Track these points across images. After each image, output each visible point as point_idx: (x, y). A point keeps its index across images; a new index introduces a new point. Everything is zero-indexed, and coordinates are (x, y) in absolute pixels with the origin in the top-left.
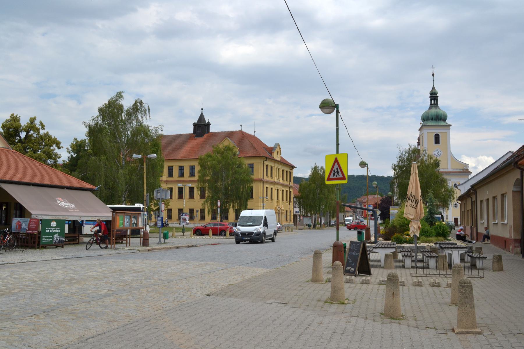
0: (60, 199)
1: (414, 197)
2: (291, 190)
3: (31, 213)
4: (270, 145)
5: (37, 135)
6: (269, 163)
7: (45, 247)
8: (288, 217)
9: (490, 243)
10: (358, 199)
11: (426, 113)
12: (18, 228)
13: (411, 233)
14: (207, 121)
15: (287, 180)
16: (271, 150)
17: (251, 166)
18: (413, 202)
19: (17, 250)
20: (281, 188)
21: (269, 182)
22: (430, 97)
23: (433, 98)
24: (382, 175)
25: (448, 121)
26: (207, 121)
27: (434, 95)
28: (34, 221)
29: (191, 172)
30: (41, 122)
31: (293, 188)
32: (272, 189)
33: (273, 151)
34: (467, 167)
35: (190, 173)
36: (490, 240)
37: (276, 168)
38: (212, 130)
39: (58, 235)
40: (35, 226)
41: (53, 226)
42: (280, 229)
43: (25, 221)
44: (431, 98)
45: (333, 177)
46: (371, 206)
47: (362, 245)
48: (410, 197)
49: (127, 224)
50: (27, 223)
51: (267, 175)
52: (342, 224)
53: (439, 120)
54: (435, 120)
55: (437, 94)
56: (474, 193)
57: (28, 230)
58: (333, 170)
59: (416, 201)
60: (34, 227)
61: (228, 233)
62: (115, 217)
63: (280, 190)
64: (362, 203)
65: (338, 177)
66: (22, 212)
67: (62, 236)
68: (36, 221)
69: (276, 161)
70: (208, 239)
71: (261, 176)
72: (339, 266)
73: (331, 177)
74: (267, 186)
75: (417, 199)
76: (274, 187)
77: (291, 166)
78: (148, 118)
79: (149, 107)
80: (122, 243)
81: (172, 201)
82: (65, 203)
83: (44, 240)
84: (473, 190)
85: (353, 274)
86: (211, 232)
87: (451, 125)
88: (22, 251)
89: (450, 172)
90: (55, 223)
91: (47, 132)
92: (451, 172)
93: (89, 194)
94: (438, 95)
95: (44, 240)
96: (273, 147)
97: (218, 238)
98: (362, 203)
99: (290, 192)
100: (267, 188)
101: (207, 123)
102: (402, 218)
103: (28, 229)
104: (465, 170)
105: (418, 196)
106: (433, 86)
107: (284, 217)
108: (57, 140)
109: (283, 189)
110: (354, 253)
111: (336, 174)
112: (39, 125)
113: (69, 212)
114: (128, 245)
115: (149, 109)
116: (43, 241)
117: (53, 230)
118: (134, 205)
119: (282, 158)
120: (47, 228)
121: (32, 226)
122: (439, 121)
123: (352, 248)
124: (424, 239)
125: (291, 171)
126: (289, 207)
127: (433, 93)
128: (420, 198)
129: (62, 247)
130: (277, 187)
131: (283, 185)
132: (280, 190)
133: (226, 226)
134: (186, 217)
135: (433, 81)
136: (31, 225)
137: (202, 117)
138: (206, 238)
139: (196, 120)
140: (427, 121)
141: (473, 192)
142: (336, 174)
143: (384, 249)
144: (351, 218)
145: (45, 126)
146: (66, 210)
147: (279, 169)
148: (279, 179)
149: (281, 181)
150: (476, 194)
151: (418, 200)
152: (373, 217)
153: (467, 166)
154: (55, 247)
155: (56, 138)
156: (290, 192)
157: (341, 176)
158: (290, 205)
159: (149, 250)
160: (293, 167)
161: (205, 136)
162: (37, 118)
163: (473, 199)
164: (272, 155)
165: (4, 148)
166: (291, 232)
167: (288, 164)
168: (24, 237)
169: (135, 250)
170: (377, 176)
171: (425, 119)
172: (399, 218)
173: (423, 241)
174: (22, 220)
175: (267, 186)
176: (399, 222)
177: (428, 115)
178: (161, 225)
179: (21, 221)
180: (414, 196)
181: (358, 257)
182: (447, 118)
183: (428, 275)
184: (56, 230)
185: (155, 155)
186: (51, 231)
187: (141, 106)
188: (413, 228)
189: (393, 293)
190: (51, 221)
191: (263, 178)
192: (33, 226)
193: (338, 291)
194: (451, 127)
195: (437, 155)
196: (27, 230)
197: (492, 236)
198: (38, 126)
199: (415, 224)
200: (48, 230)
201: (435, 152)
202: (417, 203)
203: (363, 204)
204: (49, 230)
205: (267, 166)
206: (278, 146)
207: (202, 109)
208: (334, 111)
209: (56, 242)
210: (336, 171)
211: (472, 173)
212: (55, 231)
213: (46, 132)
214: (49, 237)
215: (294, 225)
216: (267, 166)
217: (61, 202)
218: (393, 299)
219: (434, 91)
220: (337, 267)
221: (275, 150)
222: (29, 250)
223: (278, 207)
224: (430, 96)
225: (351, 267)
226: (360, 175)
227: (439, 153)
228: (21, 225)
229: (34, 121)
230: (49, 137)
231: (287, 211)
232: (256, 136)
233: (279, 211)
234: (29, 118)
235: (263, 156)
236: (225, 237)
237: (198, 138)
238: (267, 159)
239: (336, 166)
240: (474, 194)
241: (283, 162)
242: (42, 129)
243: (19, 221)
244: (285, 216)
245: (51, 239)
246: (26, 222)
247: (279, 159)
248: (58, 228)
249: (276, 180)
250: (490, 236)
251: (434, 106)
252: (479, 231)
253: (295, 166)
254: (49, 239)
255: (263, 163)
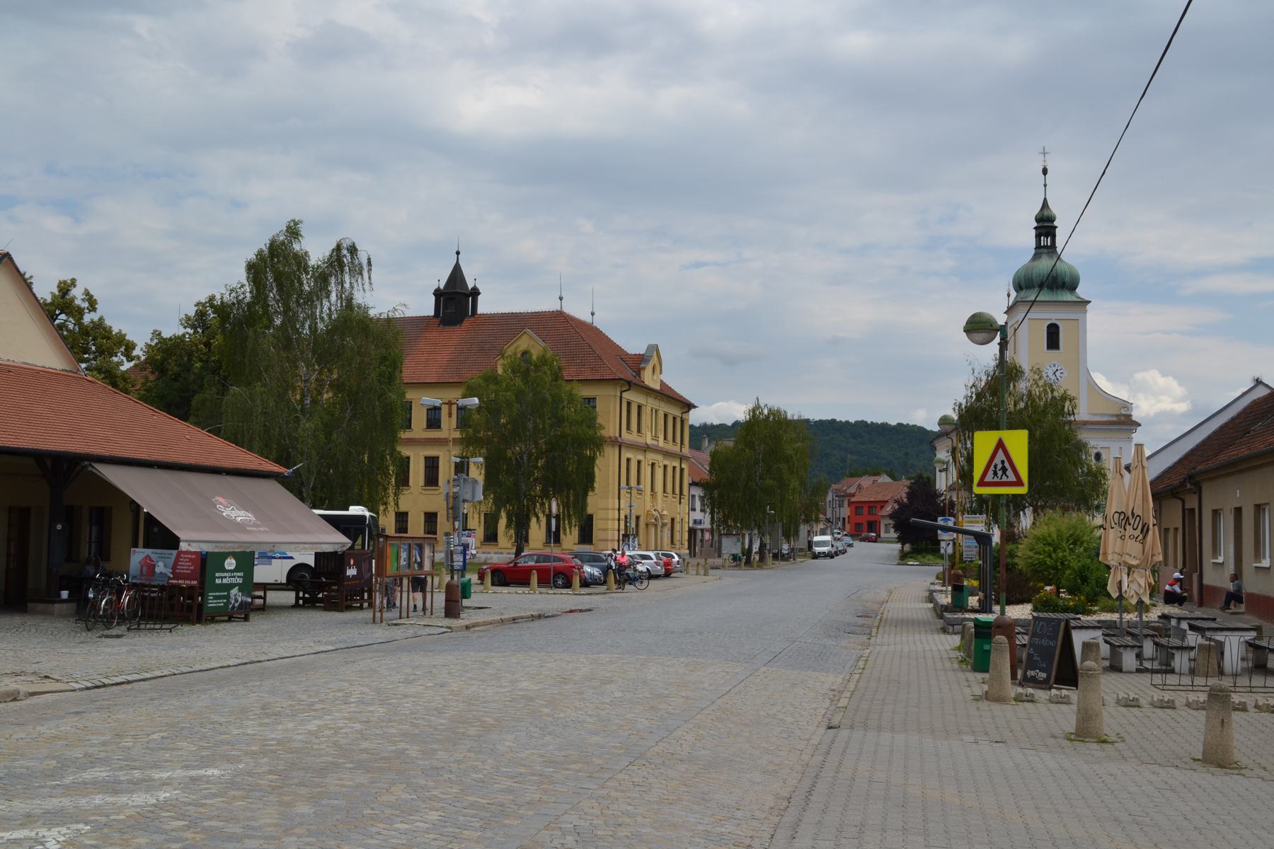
0: (221, 500)
1: (1138, 518)
2: (683, 466)
3: (179, 538)
4: (633, 345)
5: (75, 325)
6: (633, 396)
7: (212, 620)
8: (677, 536)
9: (1243, 613)
10: (833, 485)
11: (1026, 268)
12: (144, 573)
13: (1132, 596)
14: (470, 286)
15: (674, 440)
16: (638, 363)
17: (591, 401)
18: (1136, 529)
19: (158, 626)
20: (660, 460)
21: (634, 447)
22: (1035, 228)
23: (1044, 231)
24: (882, 422)
25: (1081, 291)
26: (470, 286)
27: (1046, 224)
28: (189, 556)
29: (429, 416)
30: (87, 293)
31: (687, 460)
32: (639, 462)
33: (641, 366)
34: (1128, 410)
35: (429, 421)
36: (1243, 606)
37: (650, 409)
38: (485, 306)
39: (240, 591)
40: (192, 568)
41: (230, 568)
42: (678, 569)
43: (162, 557)
44: (1039, 231)
45: (992, 480)
46: (949, 520)
47: (1063, 624)
48: (1131, 517)
49: (405, 563)
50: (171, 562)
51: (628, 428)
52: (804, 553)
53: (1057, 289)
54: (1048, 287)
55: (1054, 221)
56: (1195, 491)
57: (173, 579)
58: (993, 464)
59: (1143, 527)
60: (189, 572)
61: (576, 581)
62: (383, 547)
63: (659, 467)
64: (843, 496)
65: (1004, 479)
66: (164, 538)
67: (246, 592)
68: (194, 556)
69: (648, 391)
70: (524, 595)
71: (615, 429)
72: (1095, 670)
73: (989, 478)
74: (629, 455)
75: (1146, 524)
76: (645, 458)
77: (685, 403)
78: (367, 286)
79: (369, 259)
80: (361, 608)
81: (409, 492)
82: (233, 509)
83: (210, 601)
84: (1191, 484)
85: (1044, 686)
86: (534, 579)
87: (1090, 302)
88: (170, 629)
89: (1083, 421)
90: (234, 561)
91: (101, 319)
92: (1087, 422)
93: (273, 487)
94: (1055, 223)
95: (211, 603)
96: (643, 355)
97: (554, 594)
98: (843, 496)
99: (682, 470)
100: (628, 460)
101: (472, 289)
102: (1037, 550)
103: (171, 576)
104: (1123, 418)
105: (1149, 517)
106: (1045, 199)
107: (668, 534)
108: (127, 338)
109: (666, 462)
110: (1045, 642)
111: (1000, 473)
112: (83, 300)
113: (249, 532)
114: (428, 612)
115: (369, 263)
116: (210, 605)
117: (229, 577)
118: (348, 510)
119: (662, 383)
120: (217, 575)
121: (183, 569)
122: (1059, 292)
123: (1038, 630)
124: (1106, 603)
125: (684, 416)
126: (679, 508)
127: (1045, 218)
128: (1152, 521)
129: (246, 619)
130: (651, 457)
131: (667, 454)
132: (659, 467)
133: (567, 562)
134: (469, 538)
135: (1045, 186)
136: (181, 565)
137: (457, 275)
138: (524, 593)
139: (441, 278)
140: (1028, 291)
141: (1193, 487)
142: (1000, 473)
143: (1077, 630)
144: (828, 538)
145: (98, 302)
146: (241, 527)
147: (656, 411)
148: (655, 438)
149: (661, 443)
150: (1199, 492)
151: (1146, 526)
152: (873, 534)
153: (1128, 408)
154: (226, 618)
155: (123, 332)
156: (682, 470)
157: (1012, 478)
158: (680, 503)
159: (467, 627)
160: (688, 406)
161: (466, 323)
162: (77, 283)
163: (1186, 504)
164: (639, 375)
165: (66, 371)
166: (705, 575)
167: (671, 395)
168: (152, 595)
169: (442, 627)
170: (869, 422)
171: (1023, 285)
172: (1031, 551)
173: (1105, 608)
174: (156, 553)
175: (629, 455)
176: (1030, 561)
177: (1032, 275)
178: (461, 564)
179: (153, 557)
180: (1139, 516)
181: (1055, 649)
182: (1078, 284)
183: (1254, 690)
184: (234, 577)
185: (476, 400)
186: (225, 581)
187: (352, 258)
188: (1137, 585)
189: (1223, 720)
190: (225, 555)
191: (620, 436)
192: (187, 569)
193: (1094, 717)
194: (1089, 307)
195: (1053, 377)
196: (170, 578)
197: (1251, 596)
198: (78, 302)
199: (1142, 577)
200: (219, 578)
201: (1047, 371)
202: (1145, 530)
203: (847, 499)
204: (222, 578)
205: (629, 404)
206: (655, 353)
207: (458, 253)
208: (995, 337)
209: (234, 606)
210: (1000, 466)
211: (1140, 425)
212: (234, 581)
213: (96, 319)
214: (221, 594)
215: (691, 557)
216: (629, 404)
217: (226, 507)
218: (1223, 732)
219: (1046, 213)
220: (1090, 672)
221: (648, 364)
222: (183, 627)
223: (655, 510)
224: (1035, 224)
225: (1038, 671)
226: (824, 418)
227: (1058, 374)
228: (154, 566)
229: (68, 290)
230: (104, 329)
231: (673, 520)
232: (595, 325)
233: (655, 519)
234: (56, 283)
235: (621, 379)
236: (564, 591)
237: (447, 328)
238: (630, 386)
239: (1001, 456)
240: (1195, 493)
241: (666, 395)
242: (90, 311)
243: (148, 556)
244: (670, 532)
245: (225, 601)
246: (168, 558)
247: (658, 387)
248: (239, 574)
249: (649, 441)
250: (1244, 596)
251: (1046, 251)
252: (1206, 581)
253: (695, 404)
254: (221, 601)
255: (621, 397)
